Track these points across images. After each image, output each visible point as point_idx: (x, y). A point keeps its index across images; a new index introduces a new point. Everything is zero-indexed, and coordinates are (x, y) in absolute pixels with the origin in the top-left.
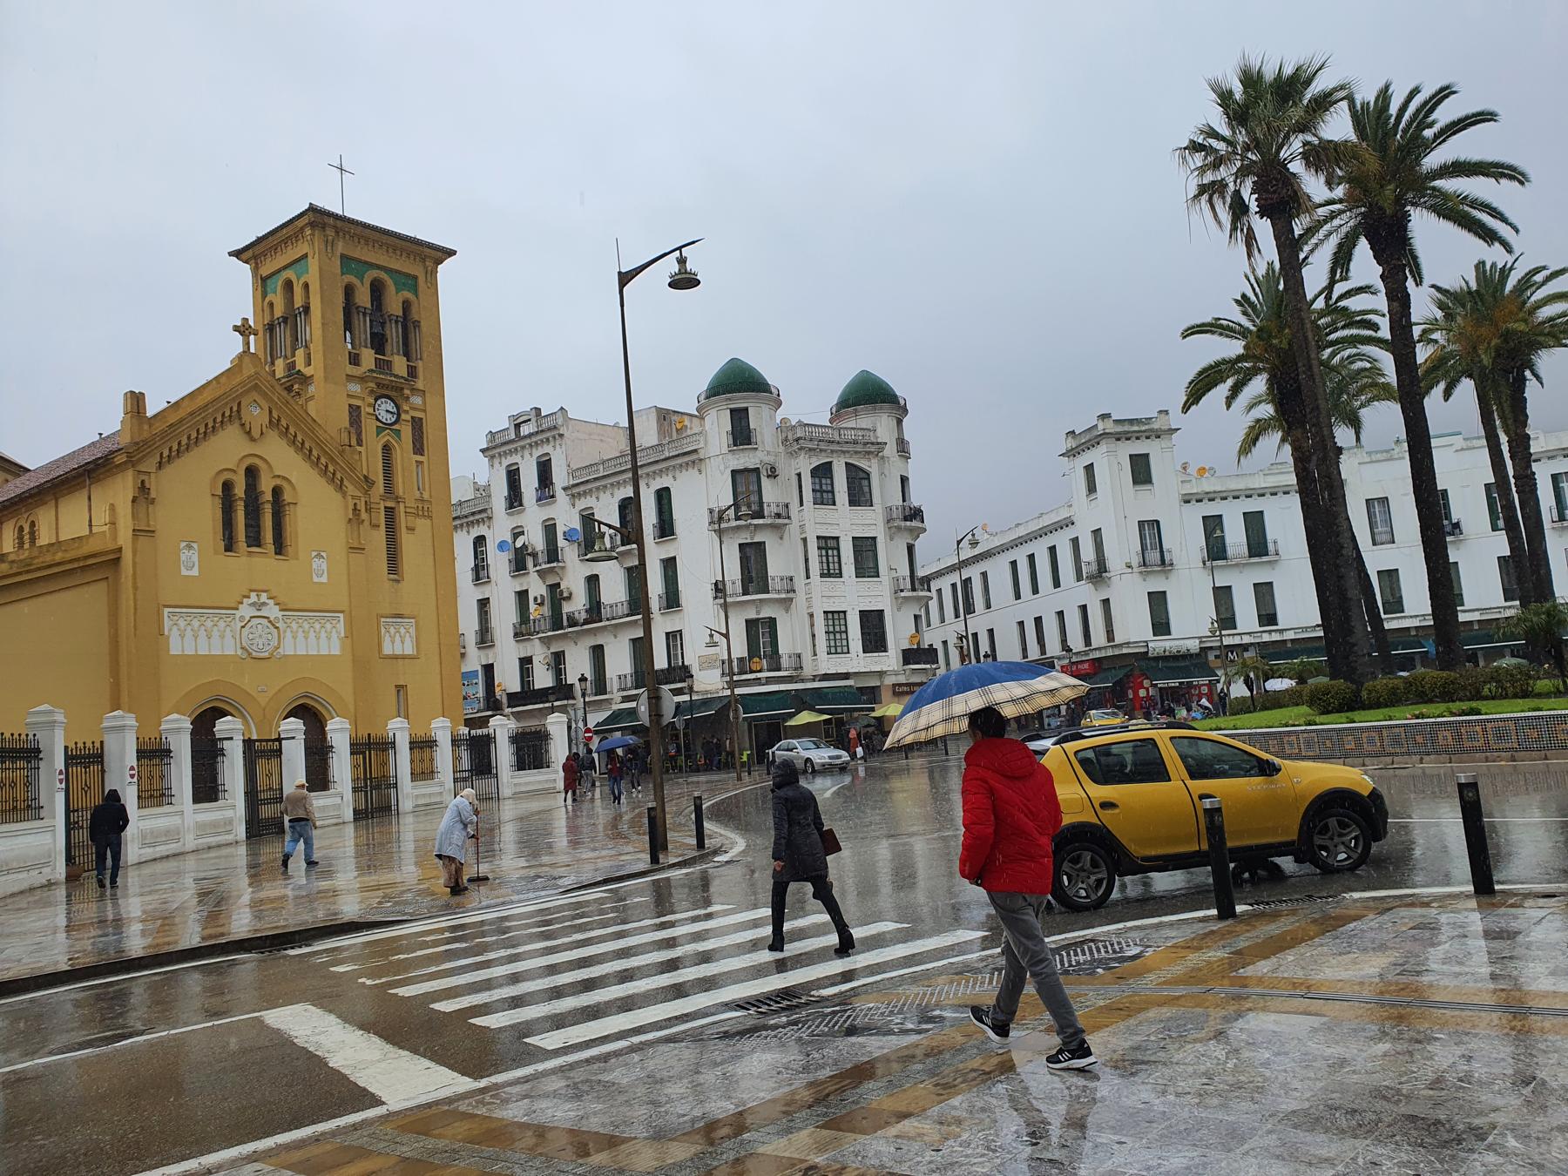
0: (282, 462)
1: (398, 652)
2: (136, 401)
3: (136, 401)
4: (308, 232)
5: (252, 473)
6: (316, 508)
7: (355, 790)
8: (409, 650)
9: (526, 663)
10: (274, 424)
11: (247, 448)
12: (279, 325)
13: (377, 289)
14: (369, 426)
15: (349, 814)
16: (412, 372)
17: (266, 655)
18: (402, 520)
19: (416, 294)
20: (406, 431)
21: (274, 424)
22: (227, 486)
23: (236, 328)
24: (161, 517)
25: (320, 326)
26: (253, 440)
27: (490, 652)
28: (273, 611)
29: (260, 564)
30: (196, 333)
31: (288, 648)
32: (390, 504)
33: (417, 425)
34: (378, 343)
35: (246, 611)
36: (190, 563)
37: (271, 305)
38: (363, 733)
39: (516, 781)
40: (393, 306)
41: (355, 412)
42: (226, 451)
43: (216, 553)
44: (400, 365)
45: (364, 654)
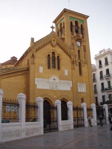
0: (58, 51)
1: (82, 91)
2: (32, 39)
3: (32, 39)
4: (64, 13)
5: (53, 53)
6: (65, 60)
7: (74, 120)
9: (103, 97)
10: (58, 44)
11: (51, 48)
12: (61, 30)
13: (76, 22)
14: (76, 47)
15: (72, 127)
16: (83, 37)
18: (82, 64)
20: (82, 47)
21: (58, 44)
22: (49, 55)
23: (51, 27)
24: (36, 60)
25: (67, 30)
26: (53, 47)
27: (97, 95)
30: (43, 28)
32: (80, 61)
33: (84, 47)
34: (77, 32)
36: (41, 69)
37: (58, 29)
38: (75, 106)
40: (80, 26)
41: (73, 44)
44: (81, 36)
45: (74, 88)
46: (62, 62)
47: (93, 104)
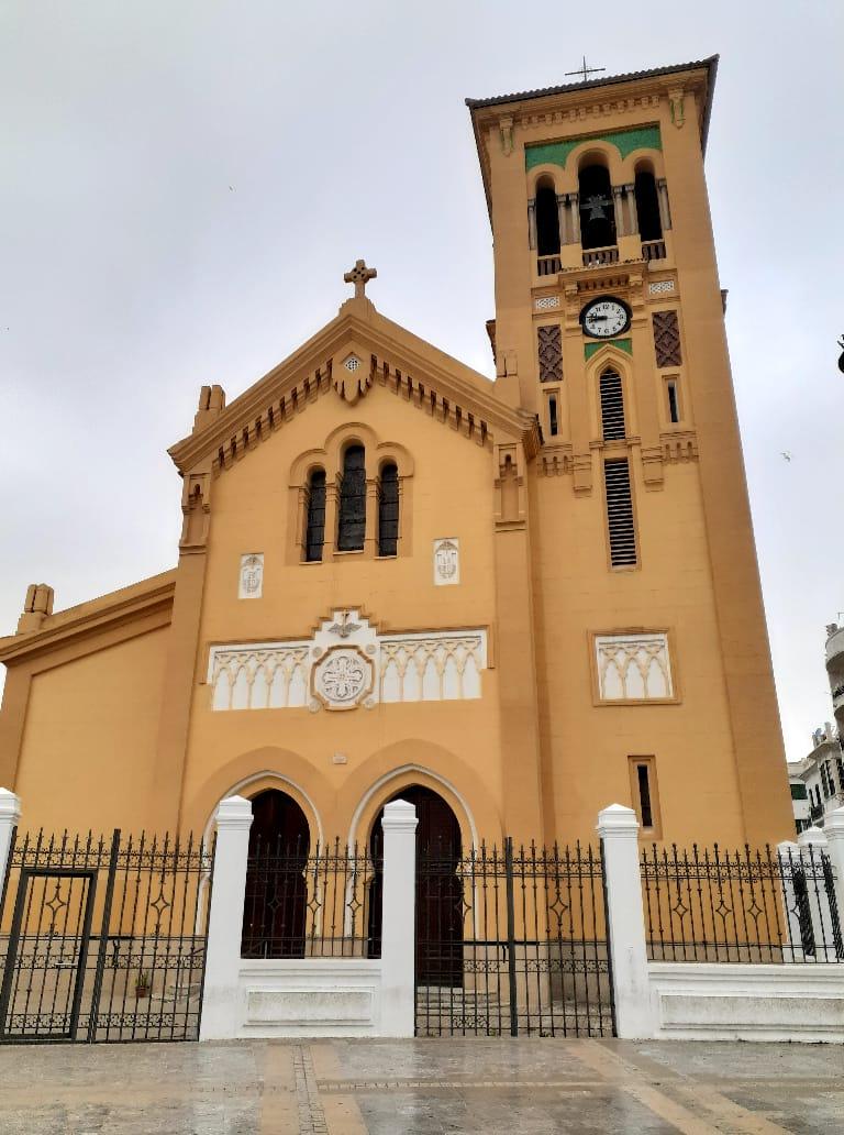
5: (353, 451)
8: (659, 688)
17: (351, 704)
19: (659, 147)
22: (317, 476)
28: (365, 636)
29: (359, 572)
31: (392, 691)
35: (324, 639)
39: (254, 986)
42: (314, 430)
43: (288, 562)
46: (416, 503)
47: (616, 807)
